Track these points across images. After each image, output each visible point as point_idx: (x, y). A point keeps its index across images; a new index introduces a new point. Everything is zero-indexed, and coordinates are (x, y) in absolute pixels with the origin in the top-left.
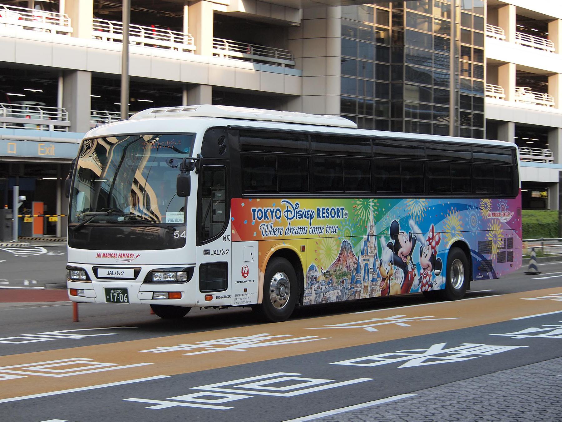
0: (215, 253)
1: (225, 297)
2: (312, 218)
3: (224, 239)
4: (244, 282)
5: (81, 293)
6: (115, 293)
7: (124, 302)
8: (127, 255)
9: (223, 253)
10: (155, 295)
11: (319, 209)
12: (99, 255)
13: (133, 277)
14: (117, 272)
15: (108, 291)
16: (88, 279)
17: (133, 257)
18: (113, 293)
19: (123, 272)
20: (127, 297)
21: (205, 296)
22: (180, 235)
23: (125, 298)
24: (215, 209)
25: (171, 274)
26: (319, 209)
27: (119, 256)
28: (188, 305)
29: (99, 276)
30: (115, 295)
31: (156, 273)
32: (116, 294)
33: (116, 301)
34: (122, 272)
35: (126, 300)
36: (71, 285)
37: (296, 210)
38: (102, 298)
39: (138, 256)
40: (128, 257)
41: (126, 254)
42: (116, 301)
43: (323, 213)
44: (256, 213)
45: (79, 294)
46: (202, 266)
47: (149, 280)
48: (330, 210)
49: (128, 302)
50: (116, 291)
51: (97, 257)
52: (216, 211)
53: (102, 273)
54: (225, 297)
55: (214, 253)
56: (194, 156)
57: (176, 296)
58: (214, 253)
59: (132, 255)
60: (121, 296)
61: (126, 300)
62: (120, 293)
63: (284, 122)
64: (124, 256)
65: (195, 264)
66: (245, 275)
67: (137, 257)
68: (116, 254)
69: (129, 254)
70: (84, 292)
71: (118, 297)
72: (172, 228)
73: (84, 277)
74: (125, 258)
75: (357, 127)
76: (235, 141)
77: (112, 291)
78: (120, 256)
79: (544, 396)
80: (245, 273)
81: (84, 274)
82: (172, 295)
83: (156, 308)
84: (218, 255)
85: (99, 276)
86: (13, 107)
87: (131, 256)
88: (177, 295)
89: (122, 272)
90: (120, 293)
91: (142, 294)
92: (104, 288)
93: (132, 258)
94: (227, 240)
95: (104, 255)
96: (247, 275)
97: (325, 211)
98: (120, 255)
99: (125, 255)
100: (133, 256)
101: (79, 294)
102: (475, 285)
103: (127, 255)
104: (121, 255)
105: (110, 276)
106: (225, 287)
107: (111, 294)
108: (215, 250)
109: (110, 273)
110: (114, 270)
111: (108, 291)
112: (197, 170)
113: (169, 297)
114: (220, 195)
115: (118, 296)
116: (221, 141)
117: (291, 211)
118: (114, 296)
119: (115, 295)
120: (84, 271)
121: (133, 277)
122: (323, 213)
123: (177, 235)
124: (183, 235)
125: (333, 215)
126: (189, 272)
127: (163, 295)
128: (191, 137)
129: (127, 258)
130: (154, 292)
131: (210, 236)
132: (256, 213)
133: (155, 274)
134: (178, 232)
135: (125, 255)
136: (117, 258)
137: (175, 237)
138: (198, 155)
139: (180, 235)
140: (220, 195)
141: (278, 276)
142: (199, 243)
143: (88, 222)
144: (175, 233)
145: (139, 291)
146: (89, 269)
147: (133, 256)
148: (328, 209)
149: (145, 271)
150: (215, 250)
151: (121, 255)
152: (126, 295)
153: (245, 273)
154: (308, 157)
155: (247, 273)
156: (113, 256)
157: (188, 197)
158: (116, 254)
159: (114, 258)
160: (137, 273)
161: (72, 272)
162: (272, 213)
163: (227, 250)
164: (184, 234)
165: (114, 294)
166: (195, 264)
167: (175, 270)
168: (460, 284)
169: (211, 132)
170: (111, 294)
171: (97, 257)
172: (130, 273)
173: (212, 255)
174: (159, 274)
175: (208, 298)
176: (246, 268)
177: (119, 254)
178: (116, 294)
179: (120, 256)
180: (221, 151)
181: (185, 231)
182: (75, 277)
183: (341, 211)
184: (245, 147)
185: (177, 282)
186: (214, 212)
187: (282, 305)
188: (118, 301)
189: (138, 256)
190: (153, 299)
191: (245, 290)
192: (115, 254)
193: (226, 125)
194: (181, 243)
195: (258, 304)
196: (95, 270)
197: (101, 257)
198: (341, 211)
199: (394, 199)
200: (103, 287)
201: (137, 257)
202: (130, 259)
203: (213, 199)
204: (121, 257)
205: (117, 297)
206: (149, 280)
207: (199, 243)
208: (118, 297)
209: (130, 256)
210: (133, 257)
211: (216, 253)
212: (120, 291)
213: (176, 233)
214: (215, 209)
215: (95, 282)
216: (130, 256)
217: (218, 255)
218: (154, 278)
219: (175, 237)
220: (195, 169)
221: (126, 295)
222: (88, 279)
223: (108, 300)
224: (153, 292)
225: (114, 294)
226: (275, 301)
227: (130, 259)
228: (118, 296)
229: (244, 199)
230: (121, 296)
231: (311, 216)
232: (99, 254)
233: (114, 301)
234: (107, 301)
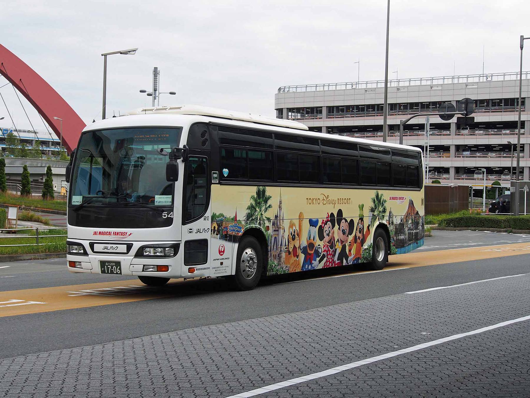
0: (198, 231)
1: (205, 269)
2: (335, 204)
3: (205, 219)
4: (221, 259)
5: (79, 265)
6: (109, 265)
7: (117, 273)
8: (121, 233)
9: (205, 232)
10: (145, 268)
11: (338, 199)
12: (95, 233)
13: (126, 252)
14: (112, 247)
15: (103, 263)
16: (85, 254)
17: (126, 236)
18: (107, 266)
19: (118, 247)
20: (120, 269)
21: (189, 269)
22: (168, 215)
23: (118, 270)
24: (197, 194)
25: (160, 250)
26: (338, 199)
27: (114, 234)
28: (168, 277)
29: (95, 251)
30: (109, 267)
31: (146, 249)
32: (110, 267)
33: (110, 272)
34: (116, 247)
35: (119, 272)
36: (70, 258)
37: (327, 199)
38: (97, 269)
39: (131, 234)
40: (122, 235)
41: (120, 232)
42: (110, 272)
43: (341, 201)
44: (308, 200)
45: (77, 266)
46: (187, 243)
47: (140, 254)
48: (344, 199)
49: (121, 273)
50: (110, 264)
51: (93, 235)
52: (198, 195)
53: (97, 247)
54: (205, 269)
55: (198, 232)
56: (181, 146)
57: (164, 269)
58: (198, 232)
59: (125, 234)
60: (115, 268)
61: (119, 272)
62: (114, 266)
63: (298, 110)
64: (118, 234)
65: (181, 241)
66: (222, 253)
67: (129, 235)
68: (110, 232)
69: (122, 233)
70: (82, 264)
71: (112, 269)
72: (161, 209)
73: (82, 251)
74: (119, 236)
75: (308, 130)
76: (217, 134)
77: (107, 264)
78: (114, 234)
79: (337, 385)
80: (222, 252)
81: (82, 249)
82: (161, 268)
83: (143, 278)
84: (201, 233)
85: (95, 251)
86: (498, 175)
87: (124, 234)
88: (165, 268)
89: (116, 247)
90: (114, 266)
91: (133, 267)
92: (99, 261)
93: (125, 236)
94: (206, 220)
95: (100, 233)
96: (224, 253)
97: (341, 200)
98: (114, 233)
99: (119, 233)
100: (126, 234)
101: (77, 266)
102: (391, 258)
103: (121, 233)
104: (116, 234)
105: (106, 251)
106: (205, 261)
107: (106, 266)
108: (199, 229)
109: (106, 248)
110: (109, 246)
111: (103, 263)
112: (184, 159)
113: (157, 269)
114: (202, 182)
115: (112, 268)
116: (203, 135)
117: (325, 200)
118: (108, 268)
119: (109, 267)
120: (82, 246)
121: (126, 252)
122: (341, 201)
123: (165, 215)
124: (171, 215)
125: (310, 203)
126: (175, 247)
127: (153, 268)
128: (178, 130)
129: (122, 236)
130: (144, 265)
131: (192, 217)
132: (308, 200)
133: (145, 249)
134: (166, 213)
135: (119, 233)
136: (112, 236)
137: (163, 217)
138: (184, 146)
139: (168, 215)
140: (202, 182)
141: (249, 251)
142: (184, 223)
143: (87, 203)
144: (163, 214)
145: (131, 264)
146: (86, 244)
147: (126, 234)
148: (343, 199)
149: (136, 246)
150: (199, 229)
151: (116, 234)
152: (119, 267)
153: (222, 252)
154: (272, 152)
155: (224, 252)
156: (108, 234)
157: (176, 182)
158: (110, 232)
159: (109, 235)
160: (129, 247)
161: (71, 246)
162: (316, 200)
163: (208, 229)
164: (171, 214)
165: (108, 266)
166: (181, 241)
167: (163, 247)
168: (381, 257)
169: (195, 126)
170: (106, 266)
171: (93, 235)
172: (123, 248)
173: (196, 233)
174: (148, 249)
175: (191, 270)
176: (222, 246)
177: (114, 232)
178: (110, 267)
179: (114, 234)
180: (204, 143)
181: (172, 212)
182: (74, 251)
183: (349, 200)
184: (223, 140)
185: (165, 256)
186: (196, 196)
187: (249, 277)
188: (112, 272)
189: (131, 234)
190: (143, 271)
191: (222, 264)
192: (110, 232)
193: (207, 122)
194: (169, 222)
195: (231, 275)
196: (92, 245)
197: (97, 235)
198: (349, 200)
199: (233, 186)
200: (99, 260)
201: (129, 235)
202: (124, 236)
203: (195, 185)
204: (115, 235)
205: (111, 269)
206: (140, 254)
207: (184, 223)
208: (112, 269)
209: (123, 234)
210: (126, 236)
211: (199, 232)
212: (114, 264)
213: (164, 214)
214: (197, 194)
215: (92, 256)
216: (123, 234)
217: (201, 233)
218: (145, 254)
219: (163, 217)
220: (182, 159)
221: (119, 267)
222: (85, 254)
223: (103, 272)
224: (143, 265)
225: (108, 266)
226: (244, 271)
227: (124, 236)
228: (112, 268)
229: (222, 186)
230: (115, 268)
231: (335, 203)
232: (96, 232)
233: (108, 273)
234: (102, 273)
